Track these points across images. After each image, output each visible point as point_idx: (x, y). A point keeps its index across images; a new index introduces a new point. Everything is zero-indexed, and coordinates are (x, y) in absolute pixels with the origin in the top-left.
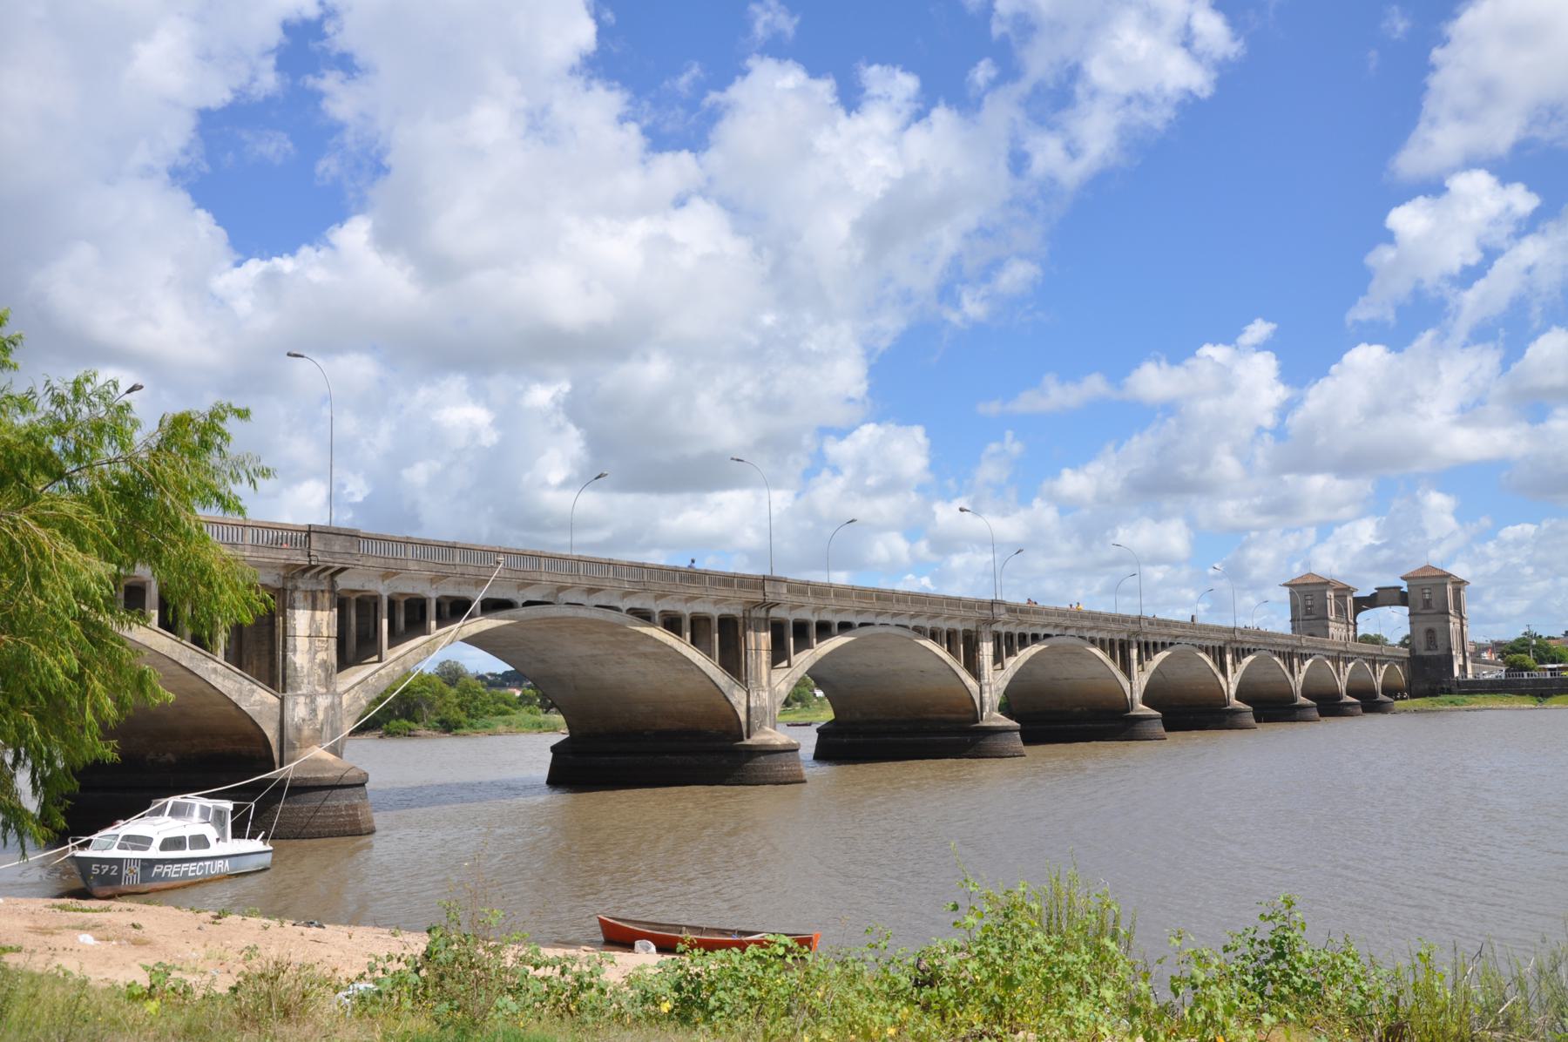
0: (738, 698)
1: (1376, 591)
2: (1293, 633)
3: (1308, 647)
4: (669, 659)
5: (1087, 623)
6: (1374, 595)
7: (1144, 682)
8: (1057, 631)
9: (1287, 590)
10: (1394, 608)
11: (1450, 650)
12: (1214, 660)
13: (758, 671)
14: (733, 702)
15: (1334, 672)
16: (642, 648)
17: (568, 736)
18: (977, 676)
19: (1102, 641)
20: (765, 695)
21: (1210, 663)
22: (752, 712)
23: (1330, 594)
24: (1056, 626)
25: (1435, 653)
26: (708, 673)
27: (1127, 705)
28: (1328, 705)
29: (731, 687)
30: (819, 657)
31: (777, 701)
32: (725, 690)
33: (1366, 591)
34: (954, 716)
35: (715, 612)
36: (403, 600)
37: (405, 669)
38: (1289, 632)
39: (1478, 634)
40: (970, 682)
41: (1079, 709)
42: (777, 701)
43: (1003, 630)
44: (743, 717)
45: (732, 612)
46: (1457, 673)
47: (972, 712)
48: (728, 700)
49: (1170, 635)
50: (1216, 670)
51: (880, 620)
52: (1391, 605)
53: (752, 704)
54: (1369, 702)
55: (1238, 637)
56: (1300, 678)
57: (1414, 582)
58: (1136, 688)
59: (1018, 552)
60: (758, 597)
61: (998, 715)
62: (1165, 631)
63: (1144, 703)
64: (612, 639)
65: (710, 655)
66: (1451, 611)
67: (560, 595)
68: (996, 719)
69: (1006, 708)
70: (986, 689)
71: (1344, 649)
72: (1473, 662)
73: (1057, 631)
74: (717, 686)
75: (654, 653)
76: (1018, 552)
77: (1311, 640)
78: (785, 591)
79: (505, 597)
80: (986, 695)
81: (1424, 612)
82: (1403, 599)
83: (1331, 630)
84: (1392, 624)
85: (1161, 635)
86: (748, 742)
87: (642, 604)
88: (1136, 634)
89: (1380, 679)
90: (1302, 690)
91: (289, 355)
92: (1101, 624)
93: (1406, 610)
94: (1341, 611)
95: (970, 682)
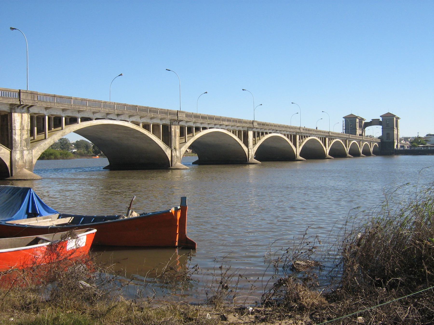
0: (168, 152)
11: (394, 140)
12: (323, 142)
15: (323, 145)
18: (247, 145)
23: (358, 120)
33: (368, 120)
35: (161, 123)
37: (54, 141)
39: (401, 136)
43: (256, 130)
46: (395, 148)
49: (309, 134)
50: (323, 145)
51: (210, 126)
55: (330, 134)
57: (384, 118)
66: (395, 127)
67: (108, 116)
70: (250, 150)
78: (185, 116)
80: (250, 153)
85: (306, 133)
89: (372, 149)
91: (167, 70)
93: (381, 127)
94: (360, 126)
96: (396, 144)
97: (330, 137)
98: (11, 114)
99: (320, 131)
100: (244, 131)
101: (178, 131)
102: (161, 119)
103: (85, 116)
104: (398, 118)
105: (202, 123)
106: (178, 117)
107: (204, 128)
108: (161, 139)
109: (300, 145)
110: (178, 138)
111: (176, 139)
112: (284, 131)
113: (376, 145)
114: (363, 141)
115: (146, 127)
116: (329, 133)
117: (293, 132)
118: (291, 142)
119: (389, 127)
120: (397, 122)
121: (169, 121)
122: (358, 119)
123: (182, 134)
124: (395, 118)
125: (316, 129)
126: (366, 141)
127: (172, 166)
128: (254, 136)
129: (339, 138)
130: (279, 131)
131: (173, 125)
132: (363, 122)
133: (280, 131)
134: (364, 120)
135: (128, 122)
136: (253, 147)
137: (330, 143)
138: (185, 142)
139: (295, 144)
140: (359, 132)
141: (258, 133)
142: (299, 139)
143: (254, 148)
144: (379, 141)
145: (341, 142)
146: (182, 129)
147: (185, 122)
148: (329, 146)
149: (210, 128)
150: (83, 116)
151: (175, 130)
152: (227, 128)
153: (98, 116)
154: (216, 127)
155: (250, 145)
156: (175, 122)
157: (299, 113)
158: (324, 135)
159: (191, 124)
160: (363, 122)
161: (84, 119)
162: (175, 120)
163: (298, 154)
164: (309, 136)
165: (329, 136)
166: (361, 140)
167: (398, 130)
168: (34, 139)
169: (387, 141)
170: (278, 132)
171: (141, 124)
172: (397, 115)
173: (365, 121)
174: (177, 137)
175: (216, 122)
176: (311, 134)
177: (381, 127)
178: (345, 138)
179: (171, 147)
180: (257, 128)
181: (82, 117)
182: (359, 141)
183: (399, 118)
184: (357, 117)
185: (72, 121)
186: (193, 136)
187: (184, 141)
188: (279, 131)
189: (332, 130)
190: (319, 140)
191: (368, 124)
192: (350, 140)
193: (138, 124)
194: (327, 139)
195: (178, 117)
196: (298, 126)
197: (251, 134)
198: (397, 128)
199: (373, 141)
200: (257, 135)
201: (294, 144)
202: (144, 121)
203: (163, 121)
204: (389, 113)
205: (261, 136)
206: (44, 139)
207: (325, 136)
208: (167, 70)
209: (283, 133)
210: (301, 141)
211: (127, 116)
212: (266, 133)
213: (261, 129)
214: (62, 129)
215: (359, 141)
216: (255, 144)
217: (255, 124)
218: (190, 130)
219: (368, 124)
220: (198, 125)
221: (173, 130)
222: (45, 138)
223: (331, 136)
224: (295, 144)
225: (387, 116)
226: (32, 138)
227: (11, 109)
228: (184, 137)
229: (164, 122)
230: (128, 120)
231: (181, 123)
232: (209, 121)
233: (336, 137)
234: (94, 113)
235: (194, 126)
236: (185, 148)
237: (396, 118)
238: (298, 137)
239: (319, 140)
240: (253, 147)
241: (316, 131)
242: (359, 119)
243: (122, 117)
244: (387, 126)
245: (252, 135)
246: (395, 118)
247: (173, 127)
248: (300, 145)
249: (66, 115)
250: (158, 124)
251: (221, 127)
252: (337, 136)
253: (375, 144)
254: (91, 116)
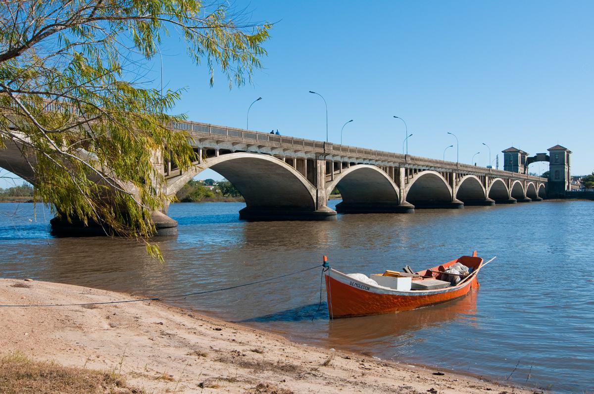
0: (313, 192)
2: (505, 170)
3: (514, 177)
4: (288, 176)
5: (439, 165)
6: (535, 157)
7: (408, 189)
8: (427, 168)
9: (503, 154)
10: (543, 162)
11: (564, 179)
12: (482, 181)
13: (321, 183)
14: (312, 194)
15: (482, 185)
16: (278, 171)
17: (341, 201)
18: (399, 186)
19: (300, 161)
20: (323, 192)
21: (480, 183)
22: (319, 199)
23: (520, 155)
24: (427, 166)
26: (303, 182)
27: (451, 199)
28: (519, 198)
29: (311, 188)
30: (343, 177)
31: (328, 194)
32: (309, 189)
33: (532, 154)
34: (389, 202)
35: (306, 157)
36: (206, 150)
37: (190, 178)
38: (501, 167)
39: (573, 173)
40: (396, 188)
41: (432, 200)
42: (328, 194)
43: (408, 167)
44: (315, 201)
45: (312, 157)
46: (566, 189)
47: (395, 198)
48: (310, 193)
49: (466, 171)
50: (482, 185)
51: (359, 161)
52: (542, 161)
53: (319, 196)
54: (533, 197)
55: (460, 168)
56: (456, 190)
57: (553, 152)
58: (454, 192)
59: (258, 99)
60: (321, 151)
61: (405, 201)
62: (466, 169)
63: (457, 198)
64: (266, 167)
65: (304, 175)
66: (566, 164)
67: (249, 148)
68: (405, 204)
69: (408, 199)
70: (402, 191)
71: (526, 178)
72: (572, 184)
73: (427, 168)
74: (306, 188)
75: (282, 173)
76: (258, 99)
77: (516, 174)
78: (332, 149)
79: (228, 149)
80: (402, 194)
81: (555, 164)
82: (546, 158)
83: (519, 170)
84: (540, 168)
85: (464, 171)
86: (317, 211)
87: (279, 153)
88: (455, 170)
89: (538, 191)
90: (527, 194)
91: (310, 92)
92: (444, 166)
93: (549, 163)
94: (523, 162)
95: (396, 188)
96: (567, 184)
97: (490, 176)
98: (399, 168)
99: (480, 169)
100: (395, 167)
101: (324, 167)
102: (306, 153)
103: (224, 148)
104: (569, 152)
105: (349, 158)
106: (324, 150)
107: (353, 164)
108: (393, 179)
109: (457, 185)
110: (323, 175)
111: (322, 177)
112: (439, 168)
113: (542, 185)
114: (528, 180)
115: (289, 161)
116: (457, 165)
117: (449, 169)
118: (392, 178)
119: (558, 164)
120: (568, 156)
121: (315, 155)
122: (520, 153)
123: (328, 171)
124: (566, 152)
125: (475, 165)
126: (531, 180)
127: (317, 209)
128: (406, 175)
129: (501, 176)
130: (392, 163)
131: (318, 159)
132: (526, 157)
133: (435, 167)
134: (527, 155)
135: (271, 155)
136: (405, 188)
137: (491, 183)
138: (332, 180)
139: (451, 184)
140: (521, 169)
143: (407, 188)
144: (546, 180)
145: (503, 181)
146: (328, 164)
147: (331, 155)
148: (488, 186)
149: (359, 164)
150: (222, 148)
151: (321, 166)
152: (377, 163)
153: (238, 147)
154: (365, 162)
156: (321, 156)
157: (455, 146)
158: (483, 173)
159: (338, 159)
160: (526, 157)
161: (224, 152)
162: (321, 154)
163: (455, 196)
164: (467, 174)
165: (490, 174)
166: (537, 181)
167: (569, 166)
168: (168, 175)
169: (556, 180)
170: (433, 168)
172: (569, 149)
173: (528, 156)
174: (323, 174)
175: (365, 156)
176: (469, 172)
177: (549, 163)
178: (507, 176)
179: (316, 186)
180: (409, 164)
181: (221, 149)
182: (523, 181)
183: (570, 152)
184: (519, 151)
185: (211, 153)
186: (340, 173)
187: (331, 180)
188: (392, 163)
189: (461, 162)
190: (477, 179)
191: (531, 160)
192: (513, 179)
193: (281, 159)
194: (487, 178)
195: (324, 150)
196: (455, 161)
197: (403, 171)
198: (568, 165)
199: (539, 181)
200: (410, 172)
201: (449, 184)
202: (288, 154)
203: (308, 154)
204: (558, 145)
206: (179, 175)
207: (484, 175)
208: (310, 92)
209: (438, 170)
210: (458, 180)
211: (269, 148)
212: (420, 170)
213: (414, 165)
214: (199, 163)
215: (523, 180)
216: (408, 183)
218: (337, 167)
219: (531, 160)
220: (346, 160)
221: (318, 165)
222: (181, 174)
223: (491, 174)
224: (451, 184)
226: (166, 174)
227: (452, 171)
228: (330, 174)
229: (309, 156)
230: (270, 153)
231: (327, 157)
232: (358, 155)
233: (497, 175)
234: (234, 144)
235: (342, 161)
236: (330, 188)
237: (567, 152)
238: (454, 175)
239: (477, 179)
240: (405, 188)
241: (475, 168)
242: (522, 154)
243: (264, 150)
245: (404, 172)
246: (566, 152)
248: (457, 185)
249: (204, 146)
250: (302, 158)
251: (371, 162)
252: (499, 174)
253: (531, 183)
254: (229, 147)
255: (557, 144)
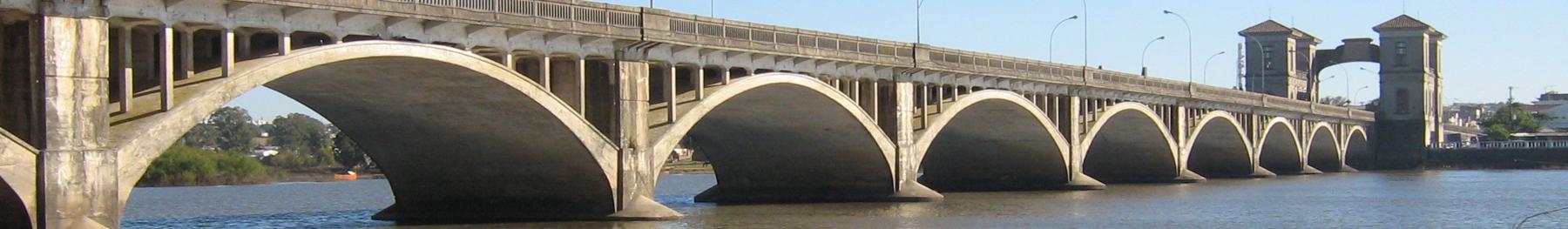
1: (1343, 44)
13: (634, 126)
25: (1405, 118)
57: (1387, 35)
93: (1376, 67)
127: (620, 208)
141: (934, 90)
142: (1082, 112)
155: (904, 131)
171: (509, 57)
177: (1376, 67)
195: (642, 32)
205: (942, 101)
210: (1089, 118)
217: (922, 57)
225: (1399, 29)
244: (1396, 66)
247: (625, 67)
255: (1268, 19)
